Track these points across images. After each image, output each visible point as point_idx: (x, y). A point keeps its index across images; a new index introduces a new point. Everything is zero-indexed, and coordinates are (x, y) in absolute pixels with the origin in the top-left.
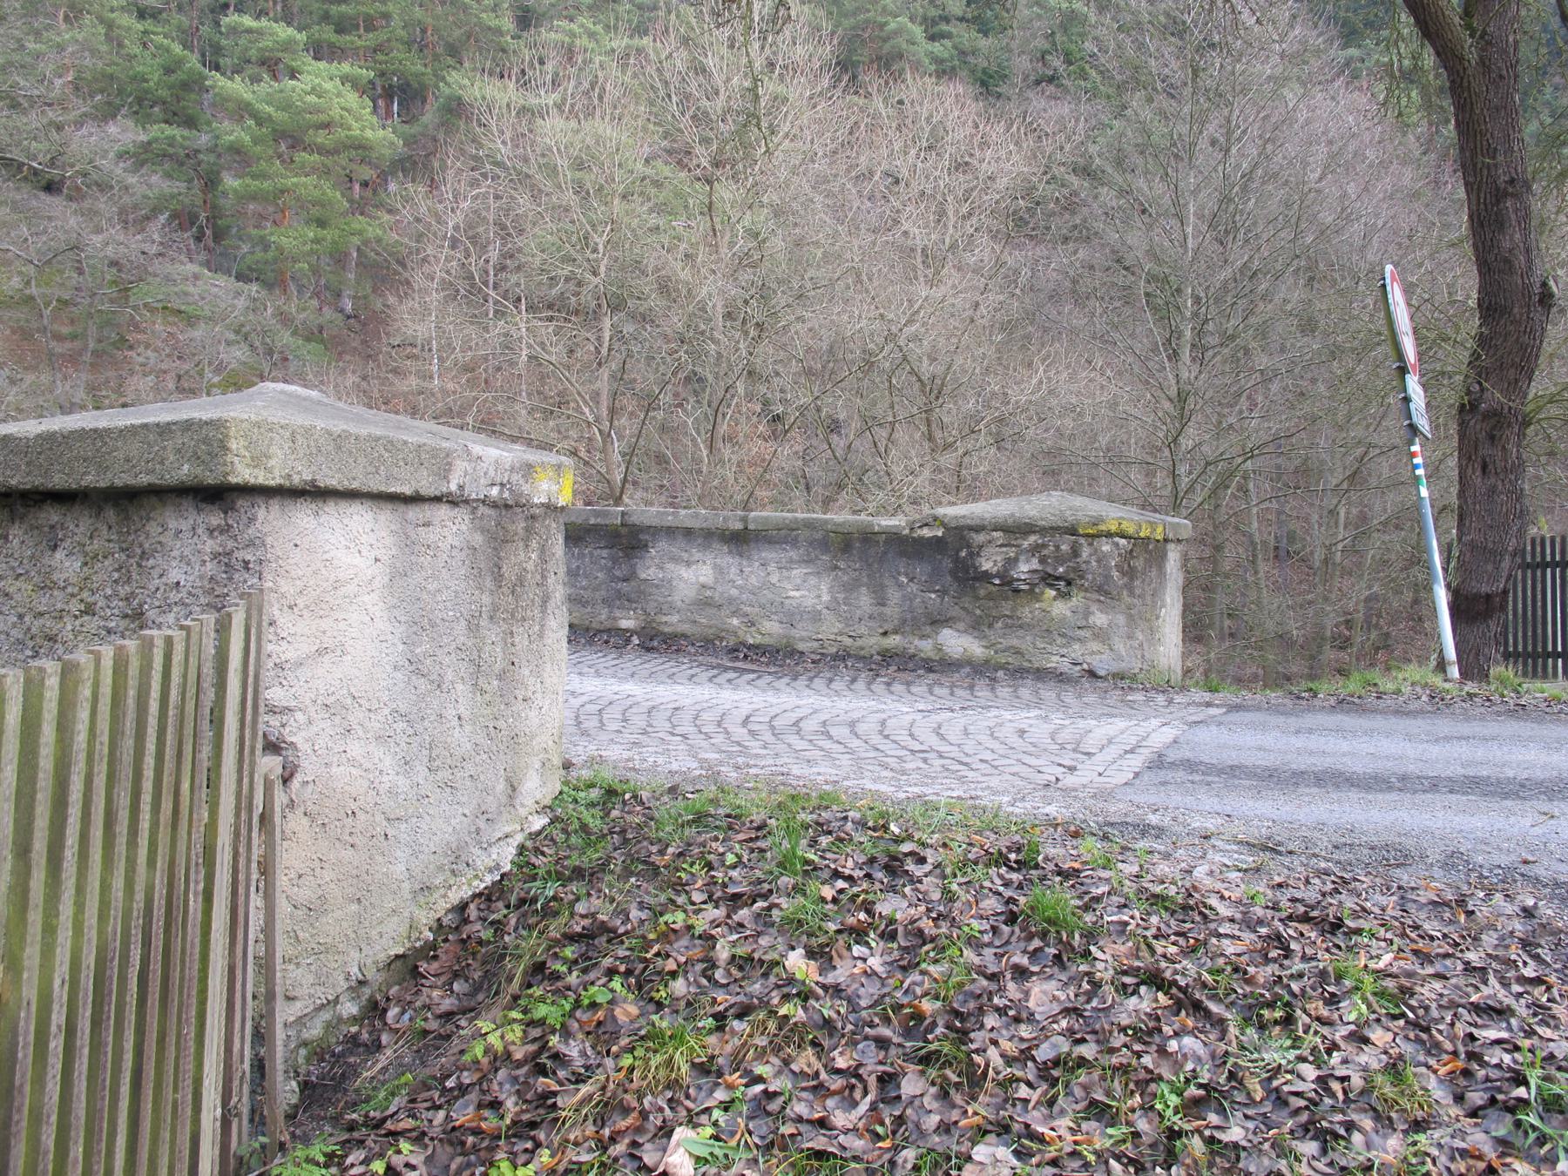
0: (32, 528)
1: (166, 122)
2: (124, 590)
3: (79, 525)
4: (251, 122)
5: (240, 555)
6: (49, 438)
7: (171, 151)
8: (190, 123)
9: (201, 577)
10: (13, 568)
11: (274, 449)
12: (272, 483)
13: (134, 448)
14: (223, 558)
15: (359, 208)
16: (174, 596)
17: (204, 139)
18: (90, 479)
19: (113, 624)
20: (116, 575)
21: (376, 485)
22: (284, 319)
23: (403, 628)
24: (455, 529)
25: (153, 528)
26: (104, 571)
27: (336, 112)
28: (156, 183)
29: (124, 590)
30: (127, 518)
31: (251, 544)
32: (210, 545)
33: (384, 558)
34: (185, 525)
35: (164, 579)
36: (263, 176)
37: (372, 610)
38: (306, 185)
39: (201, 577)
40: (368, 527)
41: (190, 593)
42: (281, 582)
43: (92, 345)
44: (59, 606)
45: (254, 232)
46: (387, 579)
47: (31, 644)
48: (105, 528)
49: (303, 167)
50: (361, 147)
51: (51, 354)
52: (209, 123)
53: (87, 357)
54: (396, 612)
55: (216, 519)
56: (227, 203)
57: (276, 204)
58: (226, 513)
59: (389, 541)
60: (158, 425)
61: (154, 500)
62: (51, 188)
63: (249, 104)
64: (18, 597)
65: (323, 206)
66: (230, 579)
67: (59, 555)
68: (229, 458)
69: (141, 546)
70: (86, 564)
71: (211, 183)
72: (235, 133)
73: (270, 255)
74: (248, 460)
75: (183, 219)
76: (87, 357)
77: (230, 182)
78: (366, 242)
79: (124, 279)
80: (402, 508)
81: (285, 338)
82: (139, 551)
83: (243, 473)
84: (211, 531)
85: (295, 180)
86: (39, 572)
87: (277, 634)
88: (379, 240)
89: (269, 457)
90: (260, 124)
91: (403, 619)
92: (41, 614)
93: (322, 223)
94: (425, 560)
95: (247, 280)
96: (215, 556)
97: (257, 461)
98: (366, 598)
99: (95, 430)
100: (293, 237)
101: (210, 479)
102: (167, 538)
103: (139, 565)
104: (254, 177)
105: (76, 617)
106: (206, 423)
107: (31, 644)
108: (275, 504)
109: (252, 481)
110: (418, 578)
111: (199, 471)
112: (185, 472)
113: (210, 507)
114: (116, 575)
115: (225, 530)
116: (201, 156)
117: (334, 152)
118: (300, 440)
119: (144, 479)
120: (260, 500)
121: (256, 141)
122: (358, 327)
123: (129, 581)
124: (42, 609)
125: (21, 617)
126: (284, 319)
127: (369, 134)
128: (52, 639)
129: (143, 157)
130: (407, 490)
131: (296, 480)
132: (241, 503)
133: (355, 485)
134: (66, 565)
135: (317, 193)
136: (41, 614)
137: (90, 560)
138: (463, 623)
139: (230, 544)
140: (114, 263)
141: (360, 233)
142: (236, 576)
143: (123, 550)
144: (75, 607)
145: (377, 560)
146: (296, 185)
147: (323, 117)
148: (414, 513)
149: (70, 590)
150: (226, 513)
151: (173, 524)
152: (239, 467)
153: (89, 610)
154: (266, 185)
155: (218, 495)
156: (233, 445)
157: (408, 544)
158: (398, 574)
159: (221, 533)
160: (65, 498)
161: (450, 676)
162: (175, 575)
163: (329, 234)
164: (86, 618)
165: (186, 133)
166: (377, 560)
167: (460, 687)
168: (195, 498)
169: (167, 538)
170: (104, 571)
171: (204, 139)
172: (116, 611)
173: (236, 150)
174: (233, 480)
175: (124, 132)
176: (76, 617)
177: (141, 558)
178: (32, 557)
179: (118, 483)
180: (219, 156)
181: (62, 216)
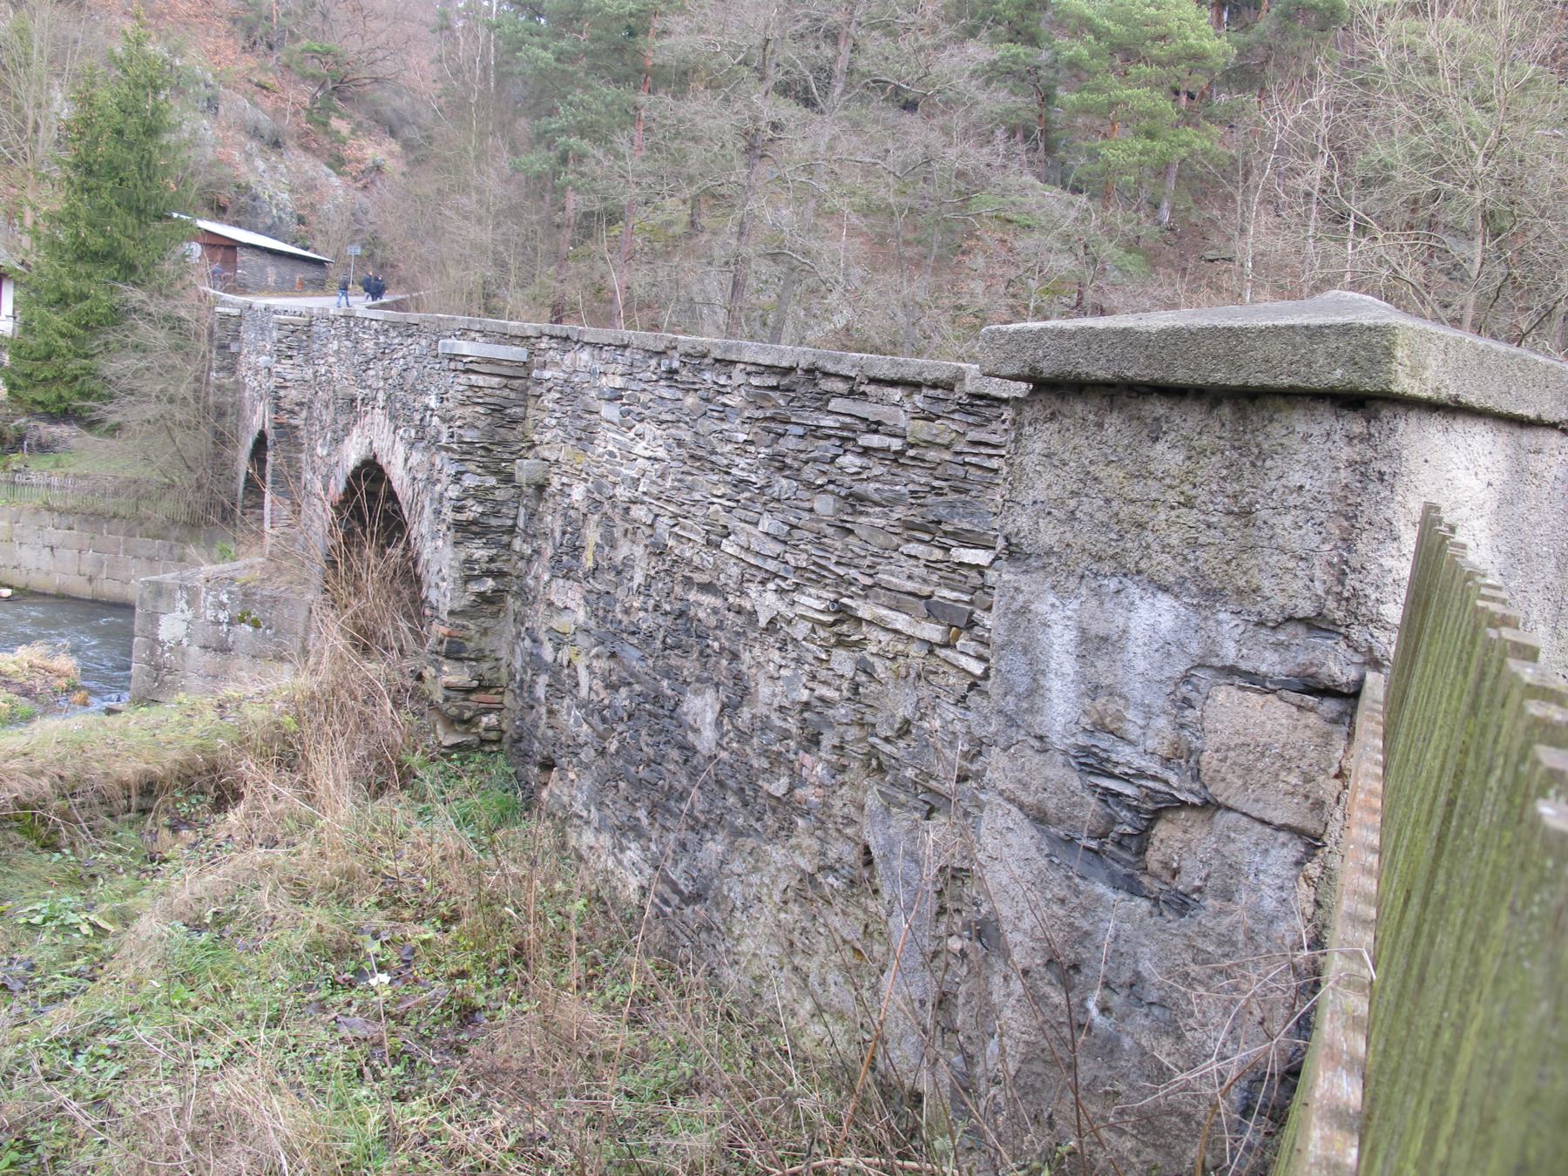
0: (1131, 418)
1: (1011, 41)
2: (1231, 488)
3: (1187, 420)
4: (1090, 37)
5: (1377, 465)
6: (1176, 333)
7: (1015, 67)
8: (1032, 40)
9: (1331, 484)
10: (1106, 455)
11: (1430, 360)
12: (1424, 395)
13: (1276, 349)
14: (1360, 468)
15: (1188, 119)
16: (1292, 500)
17: (1044, 56)
18: (1220, 377)
19: (1214, 519)
20: (1225, 472)
21: (1507, 405)
22: (1110, 232)
23: (1501, 559)
24: (1560, 458)
25: (1276, 430)
26: (1211, 466)
27: (1173, 25)
28: (998, 100)
29: (1231, 488)
30: (1244, 417)
31: (1389, 455)
32: (1346, 453)
33: (1496, 483)
34: (1316, 430)
35: (1283, 481)
36: (1098, 89)
37: (1479, 535)
38: (1139, 96)
39: (1331, 484)
40: (1488, 448)
41: (1315, 498)
42: (1410, 497)
43: (935, 250)
44: (1153, 495)
45: (1085, 144)
46: (1495, 505)
47: (1117, 528)
48: (1218, 424)
49: (1138, 78)
50: (1197, 58)
51: (901, 257)
52: (1049, 40)
53: (930, 261)
54: (1499, 541)
55: (1358, 427)
56: (1059, 116)
57: (1109, 116)
58: (1369, 422)
59: (1503, 465)
60: (1307, 327)
61: (1280, 401)
62: (910, 106)
63: (1089, 19)
64: (1108, 482)
65: (1153, 117)
66: (1365, 488)
67: (1160, 447)
68: (1394, 366)
69: (1258, 445)
70: (1190, 458)
71: (1047, 98)
72: (1075, 49)
73: (1099, 167)
74: (1408, 370)
75: (1019, 131)
76: (930, 261)
77: (1066, 97)
78: (1192, 154)
79: (968, 185)
80: (1518, 432)
81: (1109, 250)
82: (1256, 451)
83: (1404, 384)
84: (1350, 439)
85: (1129, 92)
86: (1135, 462)
87: (1399, 550)
88: (1205, 152)
89: (1424, 368)
90: (1098, 39)
91: (1504, 549)
92: (1133, 502)
93: (1151, 135)
94: (1531, 489)
95: (1076, 190)
96: (1351, 464)
97: (1416, 371)
98: (1476, 523)
99: (1230, 329)
100: (1122, 150)
101: (1368, 386)
102: (1294, 442)
103: (1253, 465)
104: (1091, 91)
105: (1173, 508)
106: (1369, 329)
107: (1117, 528)
108: (1413, 417)
109: (1409, 391)
110: (1521, 508)
111: (1355, 377)
112: (1337, 377)
113: (1351, 414)
114: (1225, 472)
115: (1366, 438)
116: (1041, 72)
117: (1174, 60)
118: (1452, 353)
119: (1285, 381)
120: (1400, 410)
121: (1093, 55)
122: (1173, 240)
123: (1238, 480)
124: (1133, 496)
125: (1108, 501)
126: (1110, 232)
127: (1207, 44)
128: (1141, 526)
129: (993, 74)
130: (1531, 413)
131: (1444, 394)
132: (1386, 413)
133: (1490, 404)
134: (1167, 457)
135: (1149, 104)
136: (1133, 502)
137: (1195, 454)
138: (1554, 561)
139: (1370, 454)
140: (961, 174)
141: (1188, 144)
142: (1371, 486)
143: (1234, 448)
144: (1172, 497)
145: (1489, 484)
146: (1129, 97)
147: (1161, 29)
148: (1528, 438)
149: (1168, 481)
150: (1369, 422)
151: (1301, 428)
152: (1401, 376)
153: (1188, 503)
154: (1102, 98)
155: (1362, 403)
156: (1399, 353)
157: (1520, 472)
158: (1506, 502)
159: (1361, 442)
160: (1175, 393)
161: (1535, 615)
162: (1296, 478)
163: (1158, 145)
164: (1184, 510)
165: (1029, 50)
166: (1489, 484)
167: (1541, 628)
168: (1332, 403)
169: (1294, 442)
170: (1211, 466)
171: (1044, 56)
172: (1220, 507)
173: (1074, 64)
174: (1395, 389)
175: (980, 52)
176: (1173, 508)
177: (1257, 457)
178: (1128, 446)
179: (1253, 382)
180: (1057, 72)
181: (918, 132)
